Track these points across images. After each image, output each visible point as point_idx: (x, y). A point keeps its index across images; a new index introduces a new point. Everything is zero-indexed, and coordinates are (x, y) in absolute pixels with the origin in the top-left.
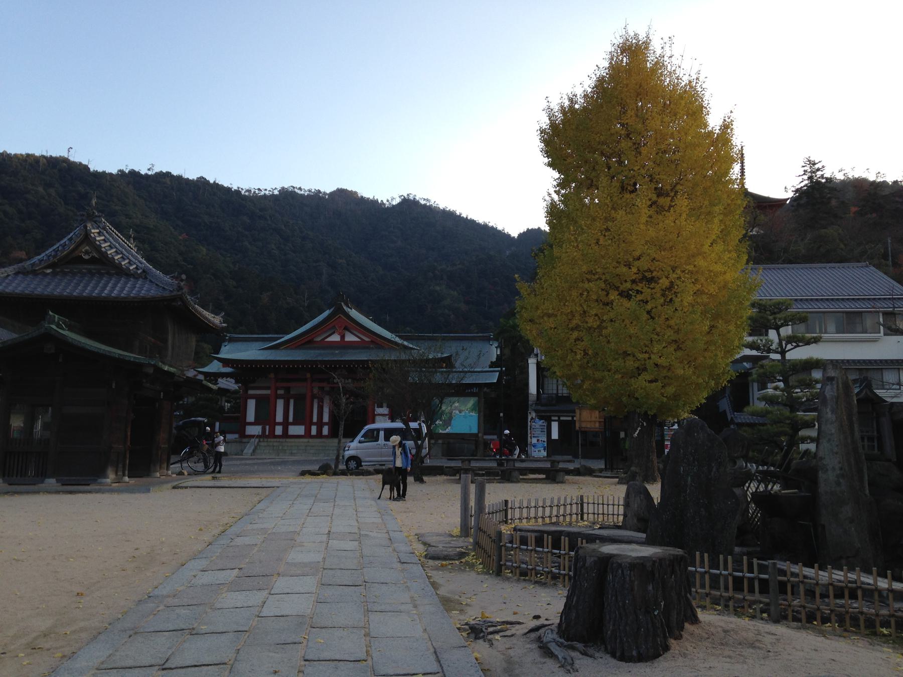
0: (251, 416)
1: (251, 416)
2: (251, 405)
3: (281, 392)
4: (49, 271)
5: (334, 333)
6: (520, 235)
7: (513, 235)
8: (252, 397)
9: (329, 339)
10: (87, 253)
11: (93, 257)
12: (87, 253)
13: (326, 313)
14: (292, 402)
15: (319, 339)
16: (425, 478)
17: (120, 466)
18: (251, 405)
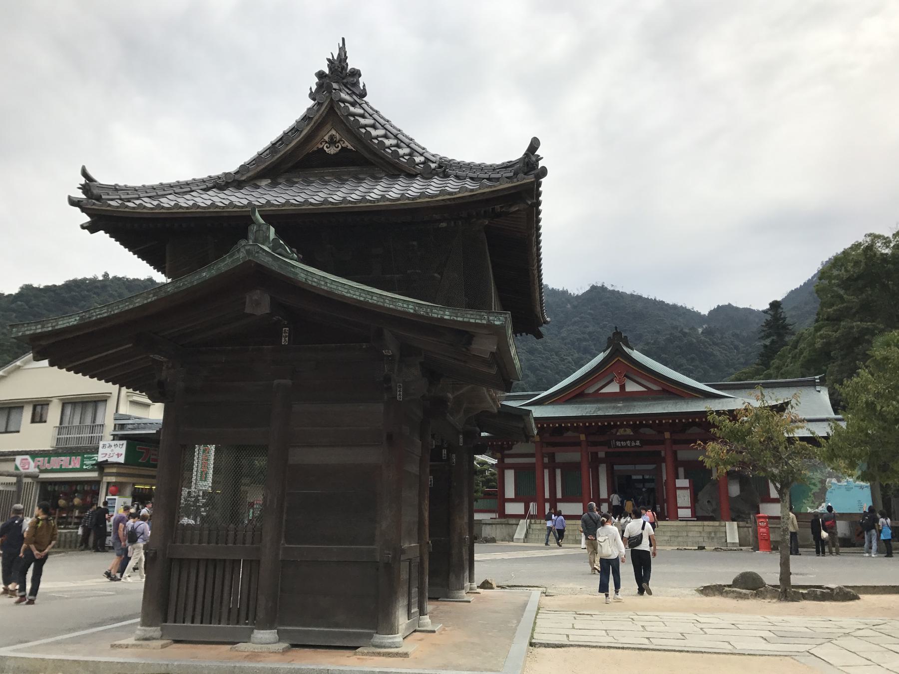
0: (510, 492)
1: (510, 492)
2: (510, 477)
5: (612, 381)
6: (711, 313)
7: (702, 313)
8: (510, 467)
9: (604, 391)
10: (332, 142)
11: (344, 149)
13: (601, 357)
14: (558, 472)
15: (591, 390)
16: (860, 596)
17: (415, 590)
18: (510, 477)
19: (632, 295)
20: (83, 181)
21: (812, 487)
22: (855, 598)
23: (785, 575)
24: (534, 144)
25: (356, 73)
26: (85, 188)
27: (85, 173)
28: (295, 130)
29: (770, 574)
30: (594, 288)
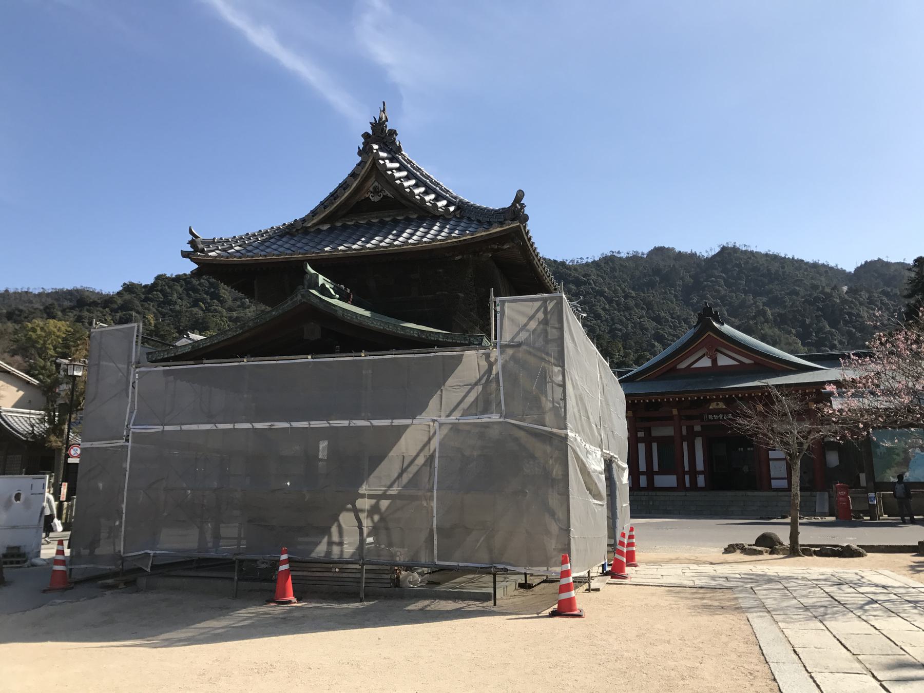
3: (641, 434)
4: (325, 227)
5: (703, 356)
7: (848, 270)
10: (376, 191)
12: (376, 191)
14: (655, 446)
15: (683, 365)
19: (767, 255)
20: (190, 237)
21: (895, 457)
22: (860, 555)
23: (794, 536)
24: (520, 196)
25: (393, 133)
26: (192, 243)
27: (191, 233)
28: (344, 186)
29: (783, 534)
30: (724, 249)
